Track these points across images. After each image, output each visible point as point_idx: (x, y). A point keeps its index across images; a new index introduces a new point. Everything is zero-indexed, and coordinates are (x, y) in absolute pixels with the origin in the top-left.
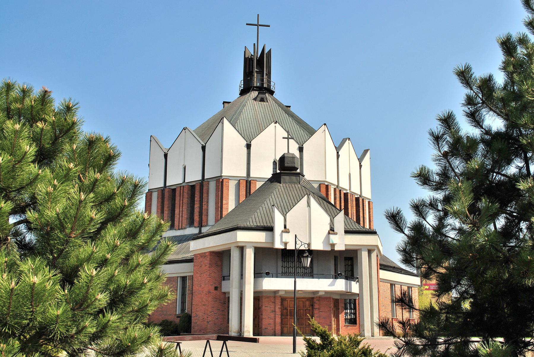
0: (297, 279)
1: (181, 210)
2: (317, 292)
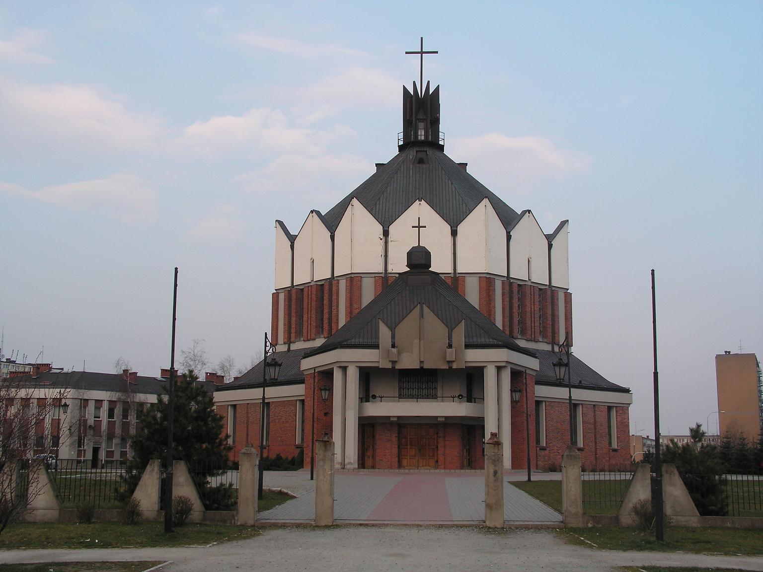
0: (571, 389)
1: (309, 315)
2: (437, 417)
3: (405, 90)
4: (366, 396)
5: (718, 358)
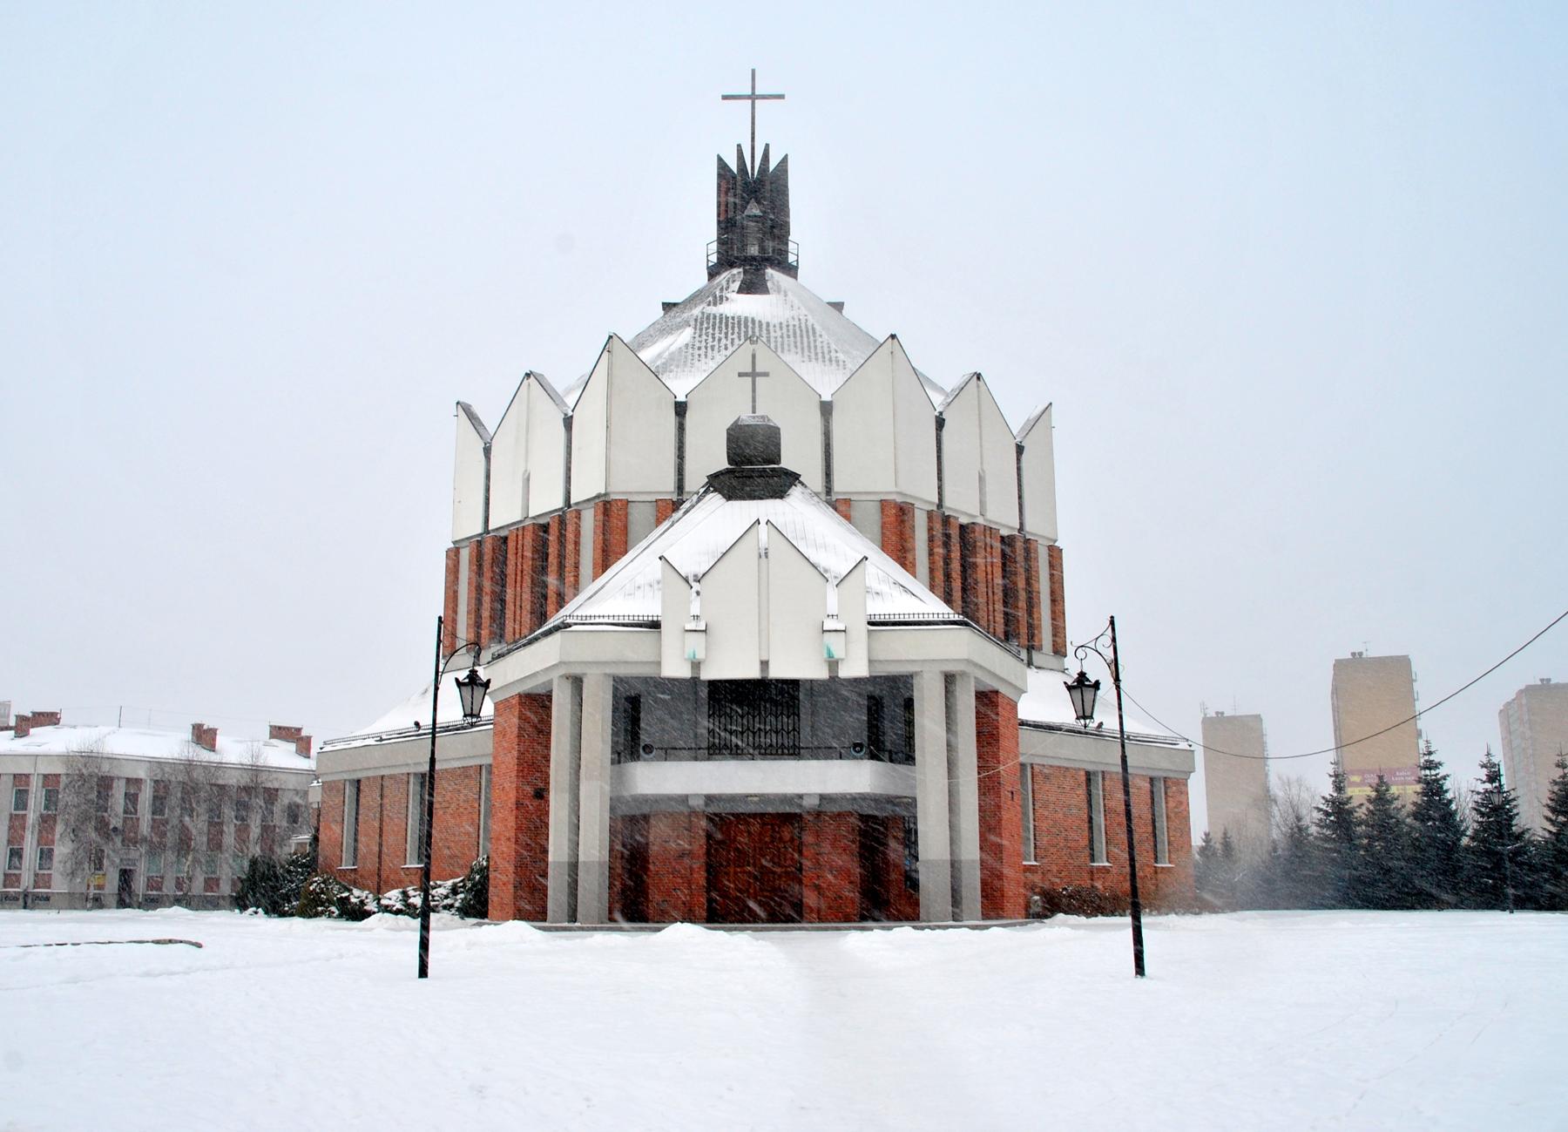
3: (722, 165)
5: (1339, 665)
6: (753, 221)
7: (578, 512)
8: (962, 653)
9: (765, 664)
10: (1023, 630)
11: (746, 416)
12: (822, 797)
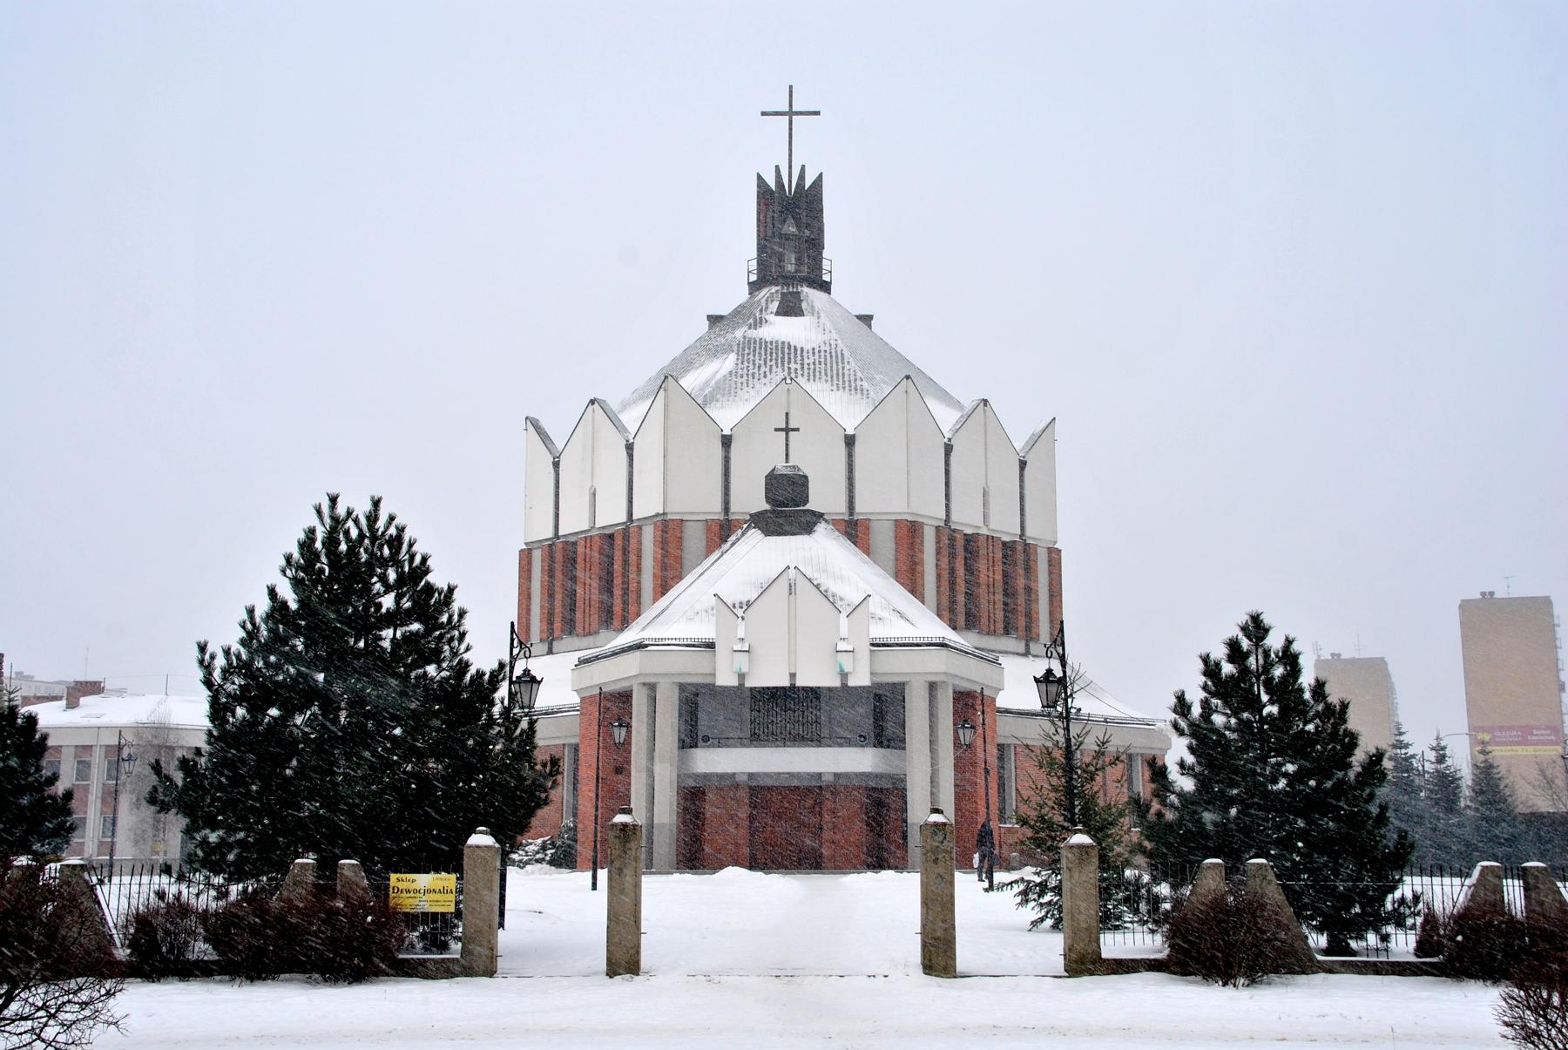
4: (691, 738)
5: (1466, 606)
6: (791, 229)
7: (640, 528)
8: (943, 669)
9: (793, 676)
10: (1022, 622)
11: (780, 465)
12: (837, 775)
